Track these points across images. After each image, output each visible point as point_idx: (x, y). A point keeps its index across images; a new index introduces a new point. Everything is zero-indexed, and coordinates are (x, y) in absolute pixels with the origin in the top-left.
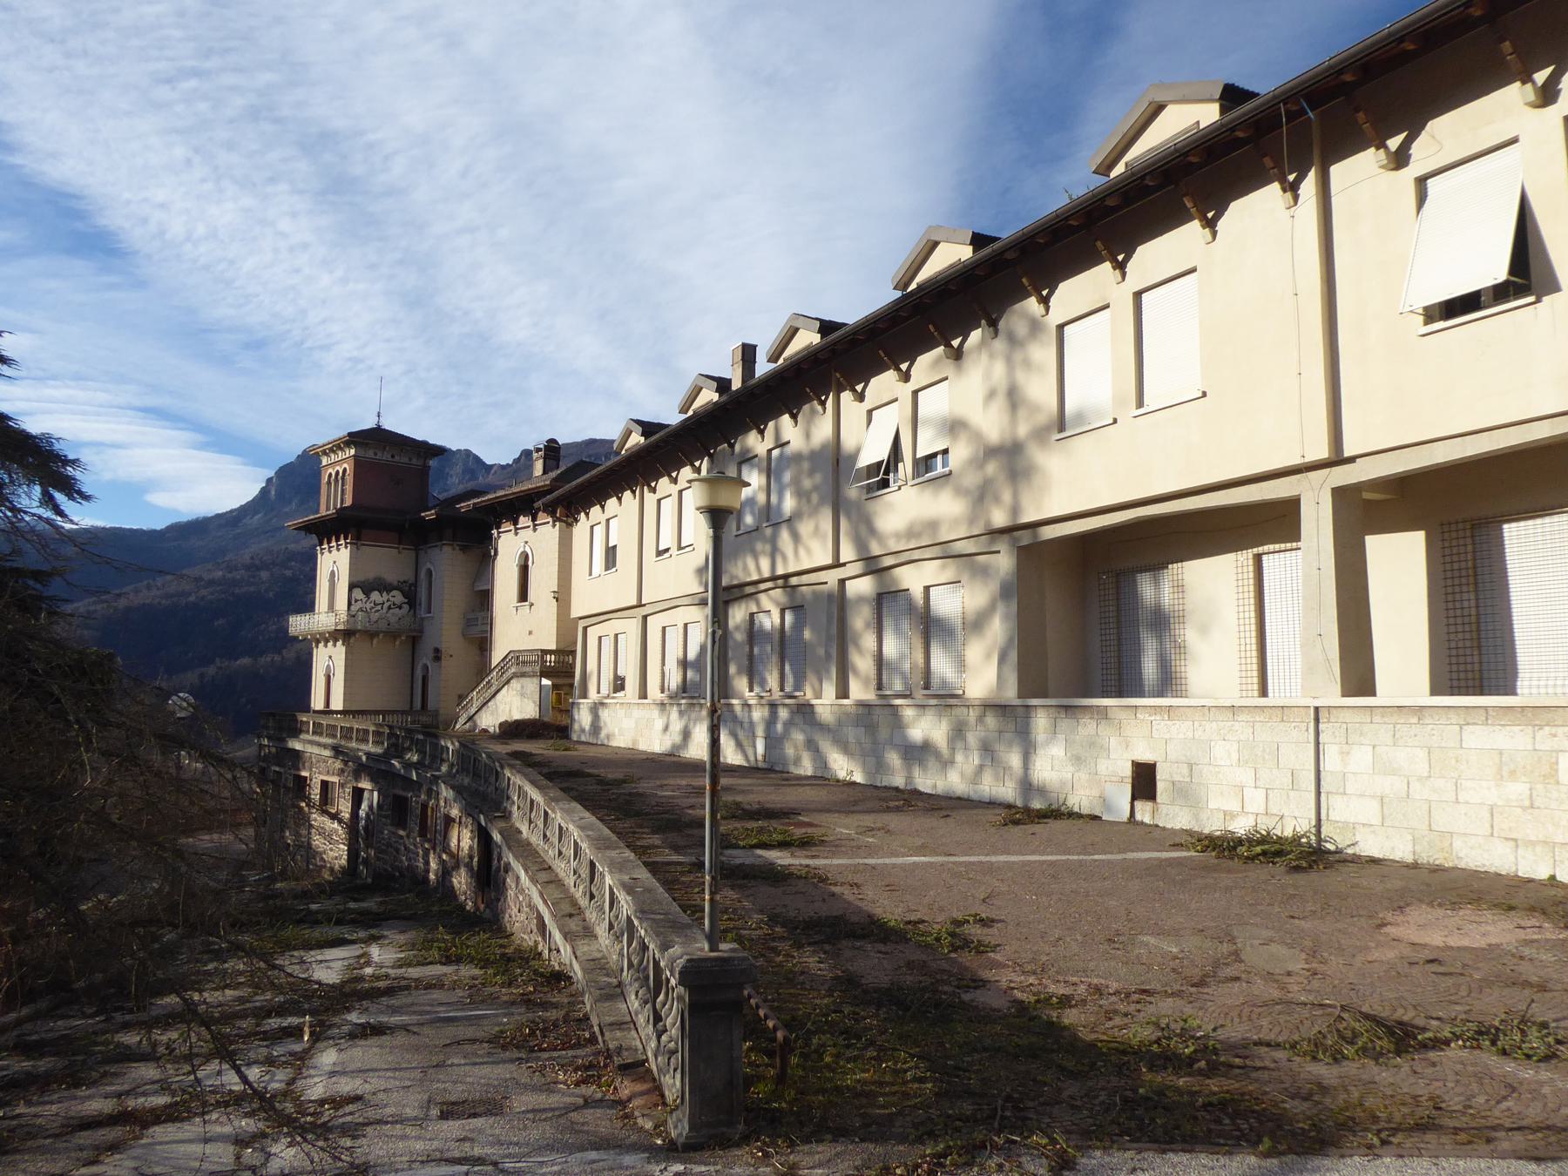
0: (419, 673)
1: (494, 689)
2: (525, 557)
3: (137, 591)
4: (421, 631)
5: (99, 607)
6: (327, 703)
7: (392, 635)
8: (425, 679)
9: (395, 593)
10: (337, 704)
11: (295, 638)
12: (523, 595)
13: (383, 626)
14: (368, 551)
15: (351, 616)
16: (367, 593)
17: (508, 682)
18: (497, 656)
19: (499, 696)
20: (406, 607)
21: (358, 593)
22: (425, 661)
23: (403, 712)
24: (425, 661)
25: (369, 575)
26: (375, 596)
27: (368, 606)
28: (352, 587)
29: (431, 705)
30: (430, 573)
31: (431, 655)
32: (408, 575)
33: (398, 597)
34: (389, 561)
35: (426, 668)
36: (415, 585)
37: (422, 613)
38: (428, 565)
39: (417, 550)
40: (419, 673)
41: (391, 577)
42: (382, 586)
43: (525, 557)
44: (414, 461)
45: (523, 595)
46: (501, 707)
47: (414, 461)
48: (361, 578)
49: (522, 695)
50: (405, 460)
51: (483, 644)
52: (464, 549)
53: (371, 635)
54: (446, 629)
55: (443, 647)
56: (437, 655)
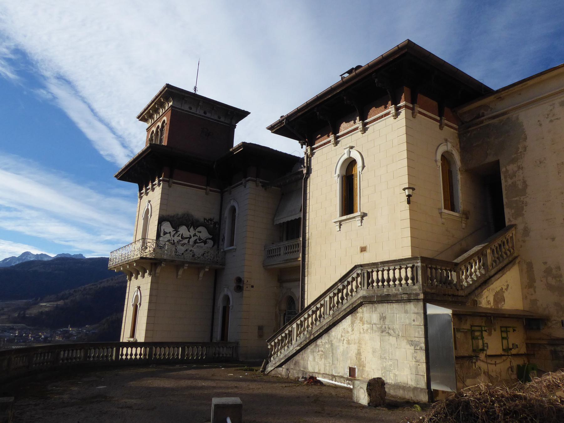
0: (220, 304)
1: (327, 320)
2: (351, 164)
3: (108, 281)
4: (224, 264)
5: (93, 287)
6: (133, 335)
7: (196, 266)
8: (226, 310)
9: (200, 229)
10: (140, 337)
11: (112, 271)
12: (348, 205)
13: (188, 257)
14: (179, 189)
15: (159, 246)
16: (176, 227)
17: (353, 311)
18: (317, 281)
19: (336, 332)
20: (210, 243)
21: (167, 227)
22: (226, 291)
23: (203, 344)
24: (226, 291)
25: (178, 210)
26: (183, 230)
27: (176, 239)
28: (161, 221)
29: (232, 336)
30: (233, 210)
31: (233, 284)
32: (213, 214)
33: (203, 233)
34: (196, 200)
35: (227, 299)
36: (219, 223)
37: (225, 247)
38: (233, 203)
39: (222, 193)
40: (220, 304)
41: (199, 214)
42: (191, 223)
43: (351, 164)
44: (222, 119)
45: (348, 205)
46: (341, 348)
47: (222, 119)
48: (171, 212)
49: (384, 331)
50: (216, 117)
51: (291, 274)
52: (264, 186)
53: (175, 265)
54: (248, 256)
55: (245, 276)
56: (239, 285)
